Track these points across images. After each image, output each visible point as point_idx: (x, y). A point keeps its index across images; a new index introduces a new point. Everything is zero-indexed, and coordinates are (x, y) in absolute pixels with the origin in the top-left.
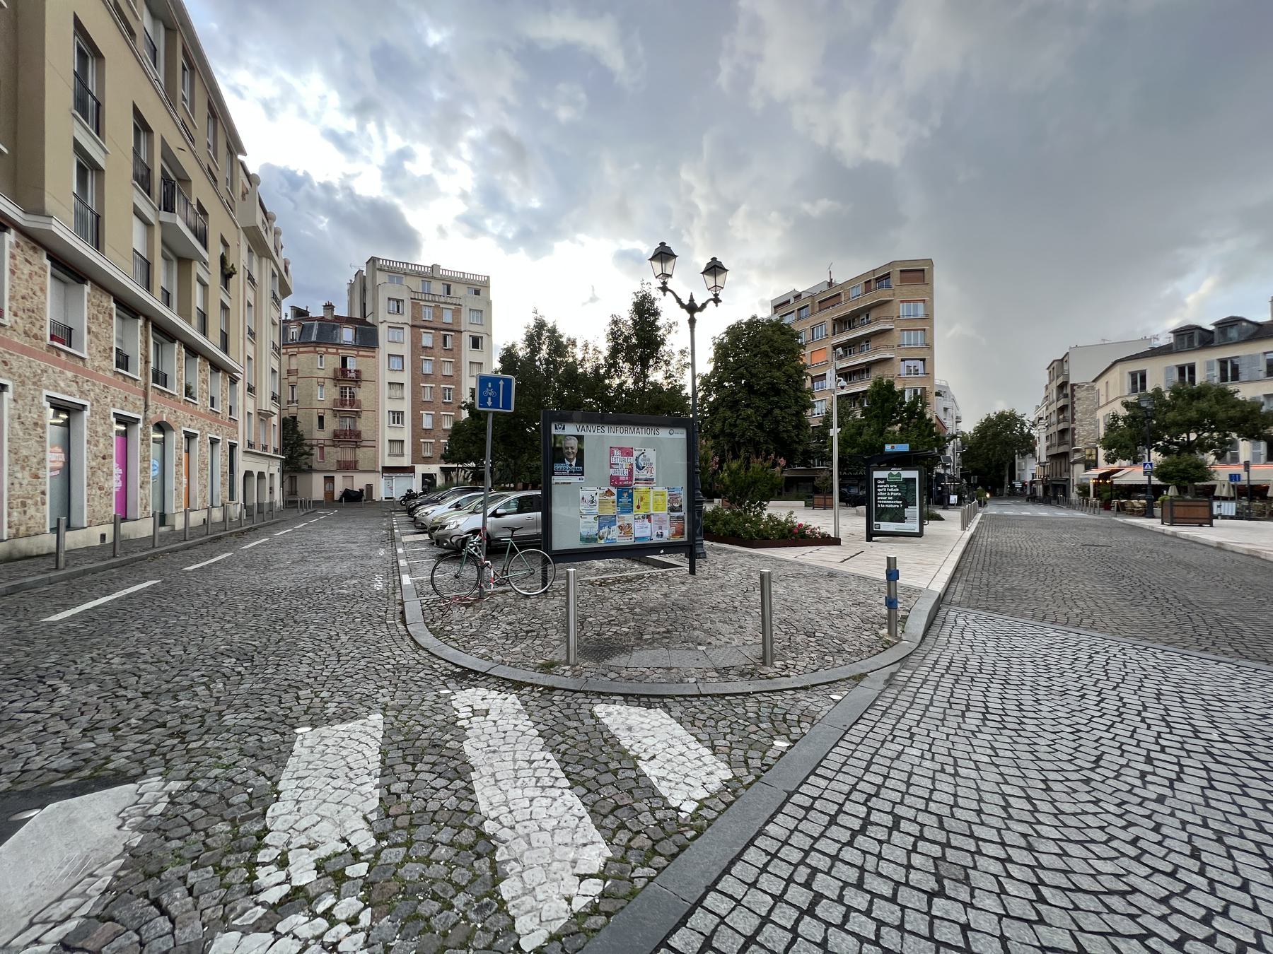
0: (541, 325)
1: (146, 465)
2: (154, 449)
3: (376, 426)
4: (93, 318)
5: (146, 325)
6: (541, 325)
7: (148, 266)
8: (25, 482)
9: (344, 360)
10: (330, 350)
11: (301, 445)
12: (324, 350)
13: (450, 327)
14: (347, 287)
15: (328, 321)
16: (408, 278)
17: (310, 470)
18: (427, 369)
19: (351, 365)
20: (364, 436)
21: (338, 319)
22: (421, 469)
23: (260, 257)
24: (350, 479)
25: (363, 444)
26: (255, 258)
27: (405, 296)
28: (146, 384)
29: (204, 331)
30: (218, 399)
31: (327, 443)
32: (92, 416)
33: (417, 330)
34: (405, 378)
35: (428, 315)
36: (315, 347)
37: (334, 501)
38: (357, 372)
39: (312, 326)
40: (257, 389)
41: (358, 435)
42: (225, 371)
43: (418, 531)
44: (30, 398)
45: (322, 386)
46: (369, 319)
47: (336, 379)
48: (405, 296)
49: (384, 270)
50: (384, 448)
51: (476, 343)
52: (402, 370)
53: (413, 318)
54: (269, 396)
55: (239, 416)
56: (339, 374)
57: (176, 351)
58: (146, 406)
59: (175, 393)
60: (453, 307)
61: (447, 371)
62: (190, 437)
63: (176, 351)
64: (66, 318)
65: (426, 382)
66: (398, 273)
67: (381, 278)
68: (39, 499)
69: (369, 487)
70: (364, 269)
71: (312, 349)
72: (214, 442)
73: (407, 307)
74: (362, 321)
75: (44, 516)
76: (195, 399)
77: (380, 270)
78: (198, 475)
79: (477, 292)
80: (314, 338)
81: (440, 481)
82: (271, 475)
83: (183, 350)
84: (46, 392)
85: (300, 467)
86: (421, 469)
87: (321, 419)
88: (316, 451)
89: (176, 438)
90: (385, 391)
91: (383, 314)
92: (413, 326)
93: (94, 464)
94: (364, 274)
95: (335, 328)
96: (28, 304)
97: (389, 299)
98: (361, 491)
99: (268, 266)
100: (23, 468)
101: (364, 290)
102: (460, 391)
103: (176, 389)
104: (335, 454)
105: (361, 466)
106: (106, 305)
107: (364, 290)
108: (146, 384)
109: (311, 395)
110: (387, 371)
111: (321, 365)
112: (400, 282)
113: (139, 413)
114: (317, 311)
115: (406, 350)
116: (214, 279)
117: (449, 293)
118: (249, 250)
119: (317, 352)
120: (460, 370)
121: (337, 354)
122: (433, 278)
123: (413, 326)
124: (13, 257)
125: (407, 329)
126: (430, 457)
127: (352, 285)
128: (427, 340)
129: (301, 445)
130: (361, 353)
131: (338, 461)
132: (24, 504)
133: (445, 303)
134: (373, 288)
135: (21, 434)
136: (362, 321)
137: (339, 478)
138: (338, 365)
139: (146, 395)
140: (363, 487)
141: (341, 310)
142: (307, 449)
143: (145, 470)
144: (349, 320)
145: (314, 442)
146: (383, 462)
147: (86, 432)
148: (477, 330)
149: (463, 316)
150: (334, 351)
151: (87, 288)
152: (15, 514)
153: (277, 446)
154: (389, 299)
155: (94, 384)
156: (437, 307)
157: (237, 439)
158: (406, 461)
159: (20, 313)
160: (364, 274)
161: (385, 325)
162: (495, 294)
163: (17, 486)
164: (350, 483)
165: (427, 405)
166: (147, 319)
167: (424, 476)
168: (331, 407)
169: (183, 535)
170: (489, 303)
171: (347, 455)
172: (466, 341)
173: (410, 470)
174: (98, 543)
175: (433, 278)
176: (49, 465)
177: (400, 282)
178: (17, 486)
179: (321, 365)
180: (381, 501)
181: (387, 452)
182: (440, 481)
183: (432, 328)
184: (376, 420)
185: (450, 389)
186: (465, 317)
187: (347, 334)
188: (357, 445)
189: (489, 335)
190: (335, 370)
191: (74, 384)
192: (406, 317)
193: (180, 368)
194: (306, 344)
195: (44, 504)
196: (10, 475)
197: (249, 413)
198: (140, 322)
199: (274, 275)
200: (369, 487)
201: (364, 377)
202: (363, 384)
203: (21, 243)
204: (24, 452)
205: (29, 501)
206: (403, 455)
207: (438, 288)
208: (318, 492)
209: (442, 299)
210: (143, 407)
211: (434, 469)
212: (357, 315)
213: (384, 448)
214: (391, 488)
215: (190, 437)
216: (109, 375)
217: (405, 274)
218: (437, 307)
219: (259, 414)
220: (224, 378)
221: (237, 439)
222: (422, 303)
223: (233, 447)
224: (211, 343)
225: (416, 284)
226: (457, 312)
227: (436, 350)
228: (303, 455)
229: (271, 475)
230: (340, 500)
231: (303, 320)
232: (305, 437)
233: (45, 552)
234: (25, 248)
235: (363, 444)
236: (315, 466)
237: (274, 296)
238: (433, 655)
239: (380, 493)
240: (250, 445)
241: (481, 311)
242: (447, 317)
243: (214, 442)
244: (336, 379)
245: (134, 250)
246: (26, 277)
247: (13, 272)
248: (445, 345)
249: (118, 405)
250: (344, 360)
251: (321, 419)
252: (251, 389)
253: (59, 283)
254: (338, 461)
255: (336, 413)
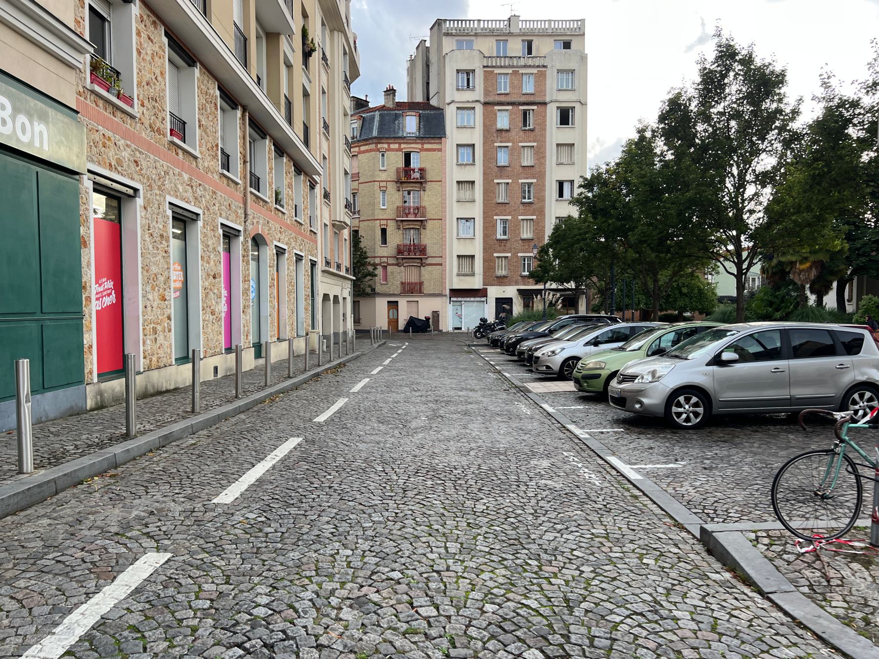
0: (727, 54)
1: (246, 286)
2: (253, 265)
3: (443, 239)
4: (202, 108)
5: (243, 115)
6: (727, 54)
7: (244, 42)
8: (155, 305)
9: (407, 157)
10: (392, 146)
11: (364, 264)
12: (386, 146)
13: (532, 99)
14: (406, 65)
15: (389, 109)
16: (480, 39)
17: (373, 294)
18: (503, 159)
19: (415, 164)
20: (430, 251)
21: (400, 105)
22: (495, 292)
23: (332, 31)
24: (414, 304)
25: (430, 261)
26: (327, 32)
27: (476, 64)
28: (245, 189)
29: (290, 120)
30: (301, 207)
31: (391, 261)
32: (204, 227)
33: (490, 108)
34: (476, 174)
35: (504, 86)
36: (377, 143)
37: (398, 331)
38: (422, 170)
39: (373, 118)
40: (331, 196)
41: (423, 250)
42: (306, 174)
43: (541, 376)
44: (156, 206)
45: (384, 192)
46: (434, 102)
47: (399, 182)
48: (476, 64)
49: (451, 35)
50: (452, 265)
51: (565, 117)
52: (473, 164)
53: (487, 92)
54: (343, 206)
55: (318, 229)
56: (402, 175)
57: (267, 149)
58: (246, 215)
59: (267, 199)
60: (535, 71)
61: (527, 160)
62: (280, 252)
63: (267, 149)
64: (179, 111)
65: (501, 177)
66: (468, 35)
67: (448, 44)
68: (166, 325)
69: (436, 314)
70: (428, 39)
71: (373, 146)
72: (299, 258)
73: (478, 80)
74: (426, 105)
75: (170, 345)
76: (282, 206)
77: (447, 34)
78: (287, 299)
79: (567, 45)
80: (375, 133)
81: (518, 308)
82: (344, 298)
83: (273, 148)
84: (170, 199)
85: (364, 290)
86: (495, 292)
87: (384, 231)
88: (379, 271)
89: (269, 253)
90: (453, 191)
91: (451, 93)
92: (486, 104)
93: (207, 284)
94: (428, 44)
95: (397, 117)
96: (152, 92)
97: (458, 71)
98: (428, 319)
99: (339, 38)
100: (153, 289)
101: (427, 66)
102: (544, 186)
103: (267, 195)
104: (399, 275)
105: (426, 289)
106: (212, 92)
107: (428, 66)
108: (245, 189)
109: (374, 204)
110: (455, 167)
111: (383, 166)
112: (470, 47)
113: (240, 224)
114: (376, 100)
115: (476, 137)
116: (296, 59)
117: (530, 52)
118: (323, 24)
119: (378, 150)
120: (544, 157)
121: (400, 150)
122: (511, 34)
123: (486, 104)
124: (139, 34)
125: (479, 108)
126: (505, 277)
127: (412, 61)
128: (503, 121)
129: (364, 264)
130: (426, 146)
131: (402, 283)
132: (155, 331)
133: (525, 66)
134: (439, 59)
135: (150, 247)
136: (426, 105)
137: (403, 303)
138: (401, 164)
139: (245, 204)
140: (429, 315)
141: (402, 96)
142: (370, 268)
143: (246, 291)
144: (411, 106)
145: (377, 261)
146: (451, 283)
147: (200, 246)
148: (566, 99)
149: (548, 82)
150: (397, 146)
151: (197, 71)
152: (148, 342)
153: (348, 266)
154: (458, 71)
155: (205, 190)
156: (515, 73)
157: (316, 257)
158: (476, 283)
159: (146, 102)
160: (428, 44)
161: (453, 107)
162: (592, 45)
163: (149, 309)
164: (415, 310)
165: (502, 208)
166: (244, 109)
167: (500, 301)
168: (394, 217)
169: (284, 369)
170: (583, 58)
171: (410, 275)
172: (552, 115)
173: (480, 293)
174: (211, 377)
175: (511, 34)
176: (173, 285)
177: (470, 47)
178: (149, 309)
179: (383, 166)
180: (448, 333)
181: (455, 270)
182: (518, 308)
183: (508, 104)
184: (443, 231)
185: (530, 185)
186: (552, 82)
187: (411, 124)
188: (422, 263)
189: (583, 104)
190: (398, 170)
191: (189, 188)
192: (478, 93)
193: (271, 169)
194: (366, 141)
195: (170, 331)
196: (143, 296)
197: (326, 225)
198: (239, 113)
199: (345, 53)
200: (436, 314)
201: (429, 176)
202: (428, 186)
203: (145, 17)
204: (154, 269)
205: (159, 328)
206: (473, 275)
207: (516, 47)
208: (382, 321)
209: (522, 62)
210: (243, 216)
211: (510, 291)
212: (419, 98)
213: (452, 265)
214: (460, 317)
215: (280, 252)
216: (216, 177)
217: (476, 35)
218: (515, 73)
219: (334, 225)
220: (305, 182)
221: (316, 257)
222: (497, 71)
223: (313, 264)
224: (295, 135)
225: (488, 46)
226: (541, 77)
227: (513, 134)
228: (366, 276)
229: (344, 298)
230: (406, 330)
231: (364, 112)
232: (369, 254)
233: (172, 387)
234: (148, 23)
235: (430, 261)
236: (379, 289)
237: (346, 80)
238: (800, 625)
239: (447, 324)
240: (328, 263)
241: (573, 71)
242: (529, 87)
243: (299, 258)
244: (399, 182)
245: (235, 24)
246: (149, 58)
247: (139, 53)
248: (525, 125)
249: (224, 215)
250: (407, 157)
251: (384, 231)
252: (326, 196)
253: (171, 65)
254: (402, 283)
255: (400, 224)
